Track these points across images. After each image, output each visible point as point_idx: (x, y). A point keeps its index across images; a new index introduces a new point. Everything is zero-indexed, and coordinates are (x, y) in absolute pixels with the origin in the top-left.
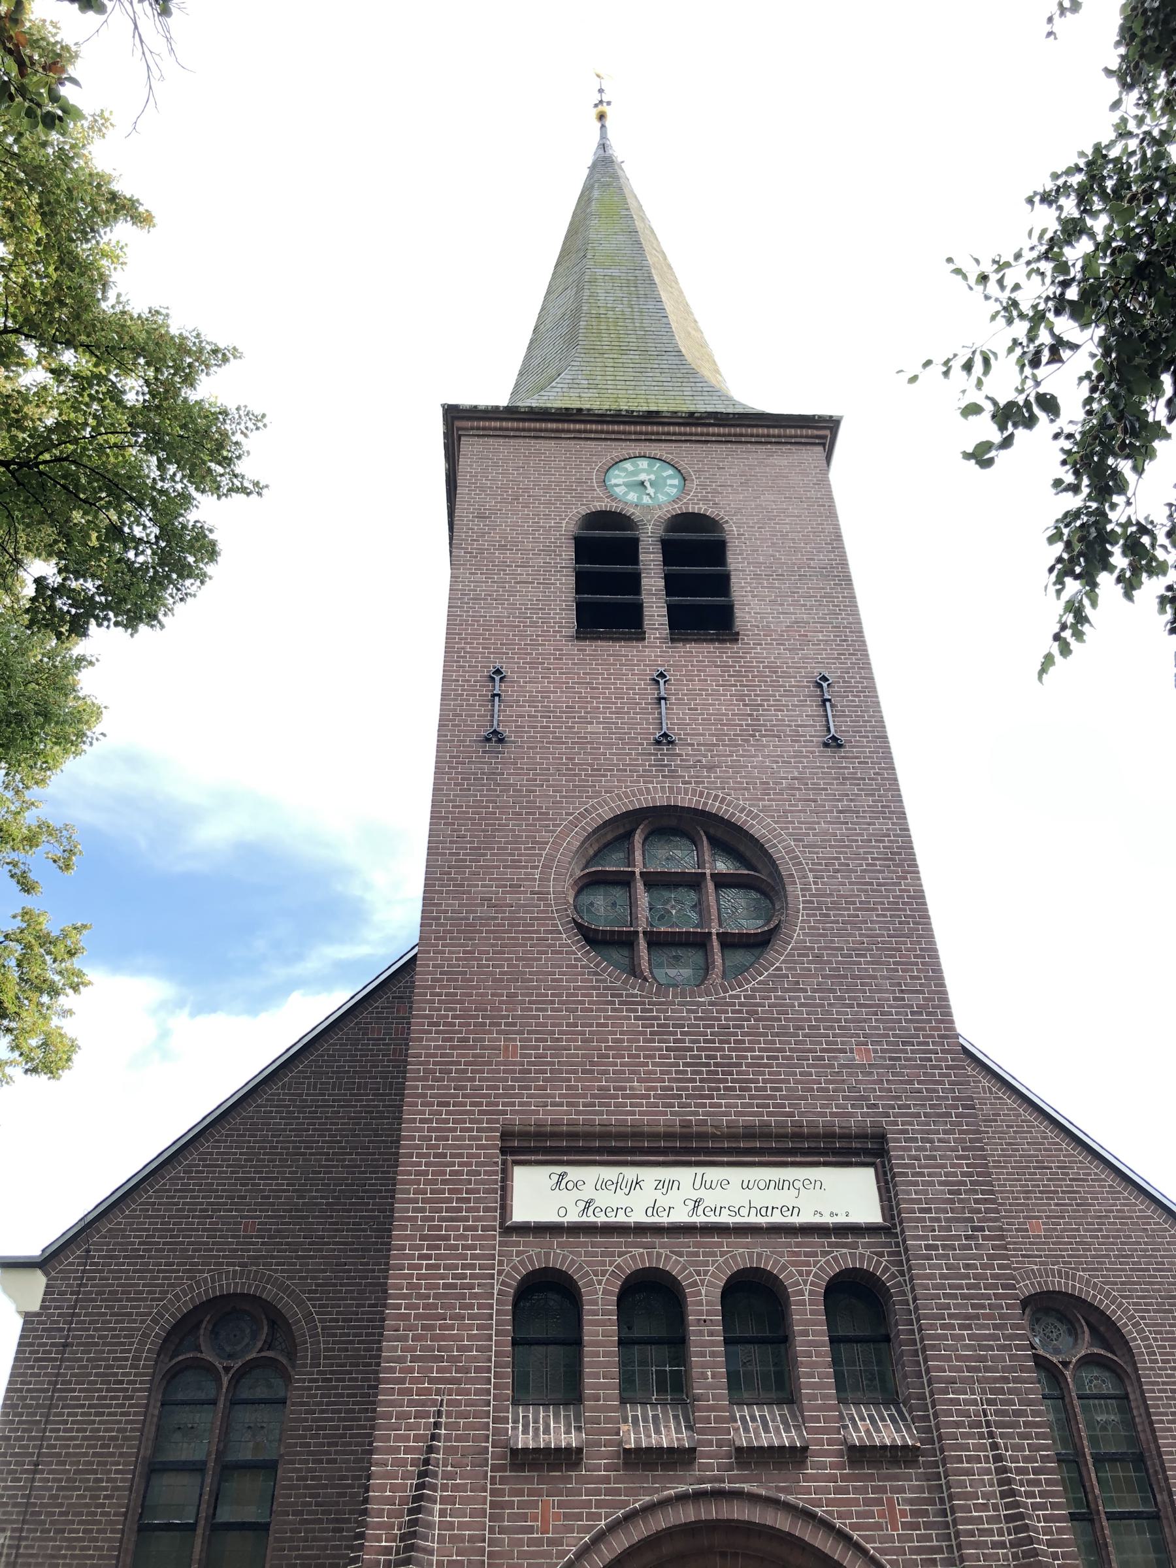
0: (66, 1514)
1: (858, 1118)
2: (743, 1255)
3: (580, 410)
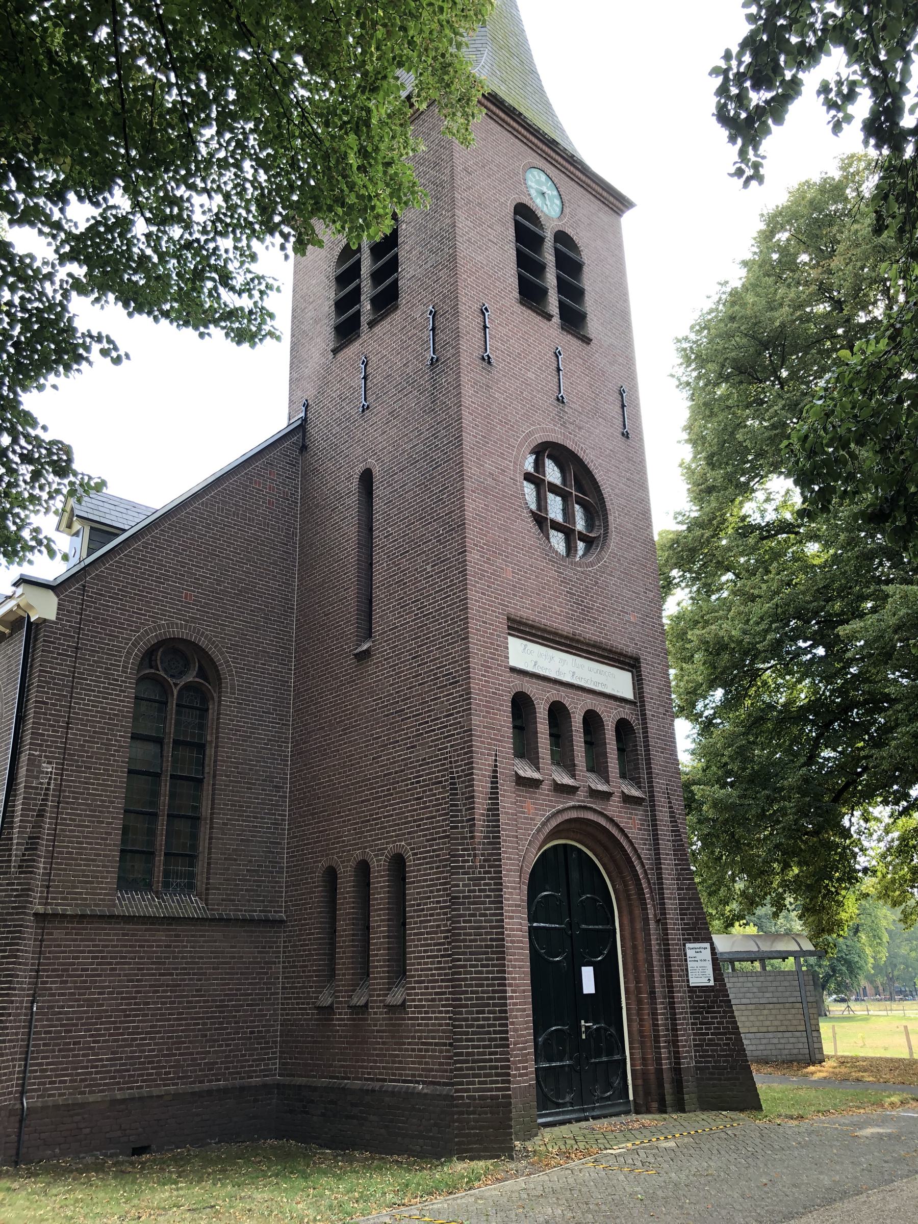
0: (91, 757)
1: (631, 650)
2: (590, 703)
3: (520, 114)
